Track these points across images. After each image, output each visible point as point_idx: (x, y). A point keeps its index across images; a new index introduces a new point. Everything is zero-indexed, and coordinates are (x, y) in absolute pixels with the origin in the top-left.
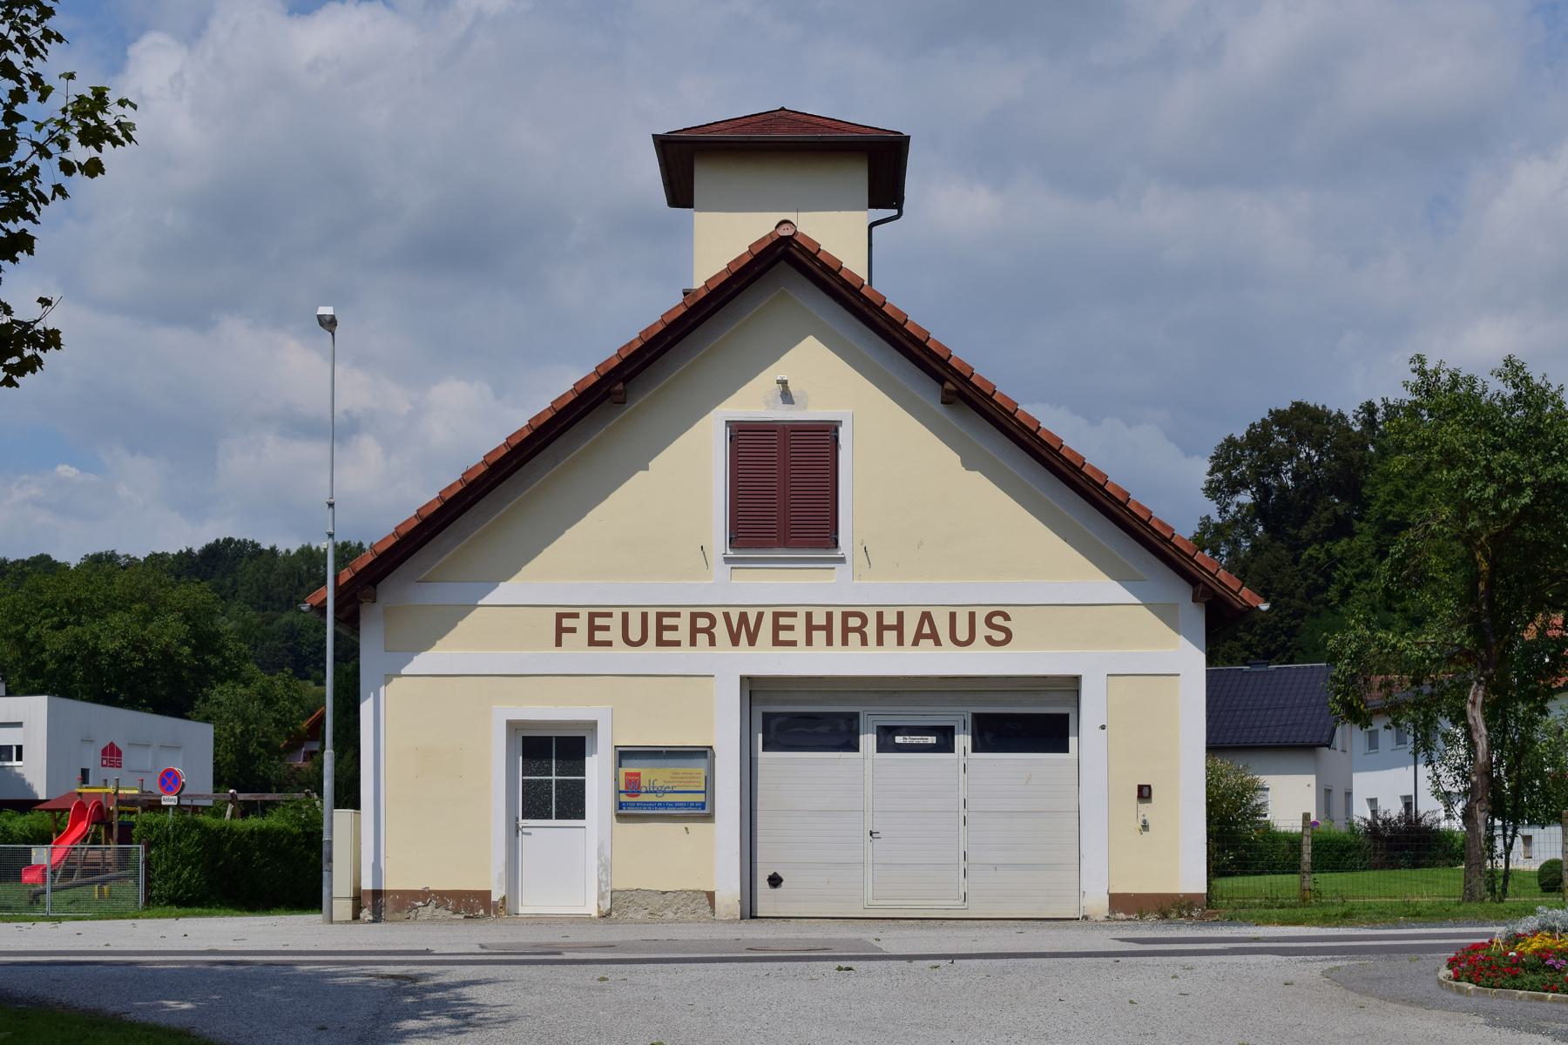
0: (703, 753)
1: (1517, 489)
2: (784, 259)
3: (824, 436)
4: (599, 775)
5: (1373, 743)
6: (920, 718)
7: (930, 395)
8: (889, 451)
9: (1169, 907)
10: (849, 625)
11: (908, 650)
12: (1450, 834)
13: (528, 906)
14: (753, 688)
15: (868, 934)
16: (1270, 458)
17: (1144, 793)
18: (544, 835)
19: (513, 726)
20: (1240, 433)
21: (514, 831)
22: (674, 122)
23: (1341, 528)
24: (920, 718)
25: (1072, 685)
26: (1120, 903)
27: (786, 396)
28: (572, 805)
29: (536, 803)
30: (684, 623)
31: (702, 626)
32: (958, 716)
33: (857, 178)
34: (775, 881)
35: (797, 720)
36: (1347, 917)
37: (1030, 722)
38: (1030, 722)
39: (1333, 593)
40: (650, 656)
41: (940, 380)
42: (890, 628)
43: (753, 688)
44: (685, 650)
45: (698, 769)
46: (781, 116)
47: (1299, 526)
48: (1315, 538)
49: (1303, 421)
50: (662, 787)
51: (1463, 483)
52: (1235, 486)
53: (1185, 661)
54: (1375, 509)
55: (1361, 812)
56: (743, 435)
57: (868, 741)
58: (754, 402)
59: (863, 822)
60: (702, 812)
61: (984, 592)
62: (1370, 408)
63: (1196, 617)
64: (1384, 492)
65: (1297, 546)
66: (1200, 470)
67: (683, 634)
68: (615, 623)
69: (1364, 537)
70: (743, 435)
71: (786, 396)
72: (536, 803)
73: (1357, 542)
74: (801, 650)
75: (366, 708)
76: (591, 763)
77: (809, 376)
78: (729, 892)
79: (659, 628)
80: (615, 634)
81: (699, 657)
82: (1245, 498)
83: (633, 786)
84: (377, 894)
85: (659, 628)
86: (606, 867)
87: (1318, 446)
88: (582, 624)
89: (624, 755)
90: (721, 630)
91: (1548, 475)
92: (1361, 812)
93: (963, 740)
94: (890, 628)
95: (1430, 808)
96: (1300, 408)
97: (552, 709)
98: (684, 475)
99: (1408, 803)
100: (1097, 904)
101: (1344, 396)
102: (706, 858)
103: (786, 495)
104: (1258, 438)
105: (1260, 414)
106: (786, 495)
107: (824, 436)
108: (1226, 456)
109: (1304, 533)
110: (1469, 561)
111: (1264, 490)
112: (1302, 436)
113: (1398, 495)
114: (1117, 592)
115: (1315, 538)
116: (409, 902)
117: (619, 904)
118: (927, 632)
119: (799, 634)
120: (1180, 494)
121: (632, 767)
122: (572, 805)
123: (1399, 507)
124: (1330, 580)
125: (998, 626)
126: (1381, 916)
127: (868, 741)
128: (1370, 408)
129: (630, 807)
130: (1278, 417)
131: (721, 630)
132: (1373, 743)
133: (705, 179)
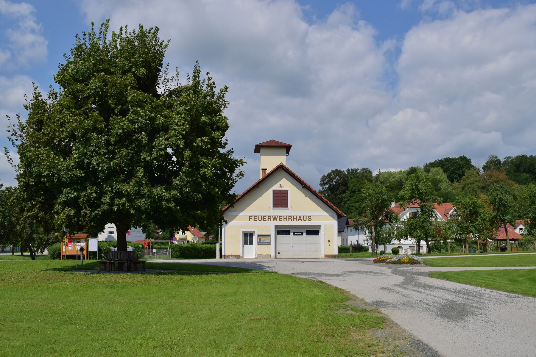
0: (270, 236)
1: (379, 200)
2: (281, 168)
3: (286, 192)
4: (255, 239)
5: (351, 231)
6: (298, 231)
7: (300, 186)
8: (295, 195)
9: (333, 256)
10: (290, 218)
11: (297, 221)
12: (365, 247)
13: (245, 257)
14: (276, 226)
15: (298, 260)
16: (331, 179)
17: (329, 241)
18: (247, 247)
19: (243, 232)
20: (326, 174)
21: (243, 246)
22: (257, 143)
23: (344, 192)
24: (298, 231)
25: (319, 226)
26: (327, 256)
27: (281, 186)
28: (251, 243)
29: (246, 243)
30: (267, 218)
31: (269, 218)
32: (304, 230)
33: (284, 151)
34: (279, 253)
35: (282, 231)
36: (357, 257)
37: (314, 231)
38: (314, 231)
39: (342, 203)
40: (262, 222)
41: (302, 185)
42: (295, 218)
43: (276, 226)
44: (267, 221)
45: (269, 238)
46: (272, 141)
47: (336, 191)
48: (339, 194)
49: (337, 172)
50: (264, 240)
51: (372, 198)
52: (325, 184)
53: (335, 223)
54: (350, 188)
55: (349, 243)
56: (275, 192)
57: (292, 234)
58: (276, 187)
59: (292, 245)
60: (269, 244)
61: (308, 213)
62: (349, 170)
63: (336, 217)
64: (351, 185)
65: (336, 195)
66: (319, 181)
67: (267, 219)
68: (257, 218)
69: (348, 194)
70: (275, 192)
71: (281, 186)
72: (246, 243)
73: (347, 194)
74: (283, 221)
75: (223, 230)
76: (254, 237)
77: (284, 184)
78: (273, 255)
79: (263, 218)
80: (257, 219)
81: (269, 222)
82: (327, 186)
83: (260, 240)
84: (225, 255)
85: (263, 218)
86: (256, 251)
87: (340, 177)
88: (253, 218)
89: (259, 236)
90: (272, 219)
91: (383, 197)
92: (349, 243)
93: (305, 234)
94: (295, 218)
95: (361, 242)
96: (336, 170)
97: (249, 230)
98: (267, 198)
99: (358, 242)
100: (323, 256)
101: (344, 169)
102: (270, 250)
103: (281, 200)
104: (329, 175)
105: (329, 171)
106: (281, 200)
107: (286, 192)
108: (323, 179)
109: (337, 193)
110: (372, 209)
111: (330, 185)
112: (337, 175)
113: (354, 186)
114: (326, 213)
115: (339, 194)
116: (229, 256)
117: (258, 256)
118: (300, 219)
119: (283, 219)
120: (317, 188)
121: (260, 237)
122: (251, 243)
123: (354, 188)
124: (342, 201)
125: (310, 218)
126: (362, 257)
127: (292, 234)
128: (349, 170)
129: (260, 243)
130: (333, 172)
131: (272, 219)
132: (351, 231)
133: (262, 150)
